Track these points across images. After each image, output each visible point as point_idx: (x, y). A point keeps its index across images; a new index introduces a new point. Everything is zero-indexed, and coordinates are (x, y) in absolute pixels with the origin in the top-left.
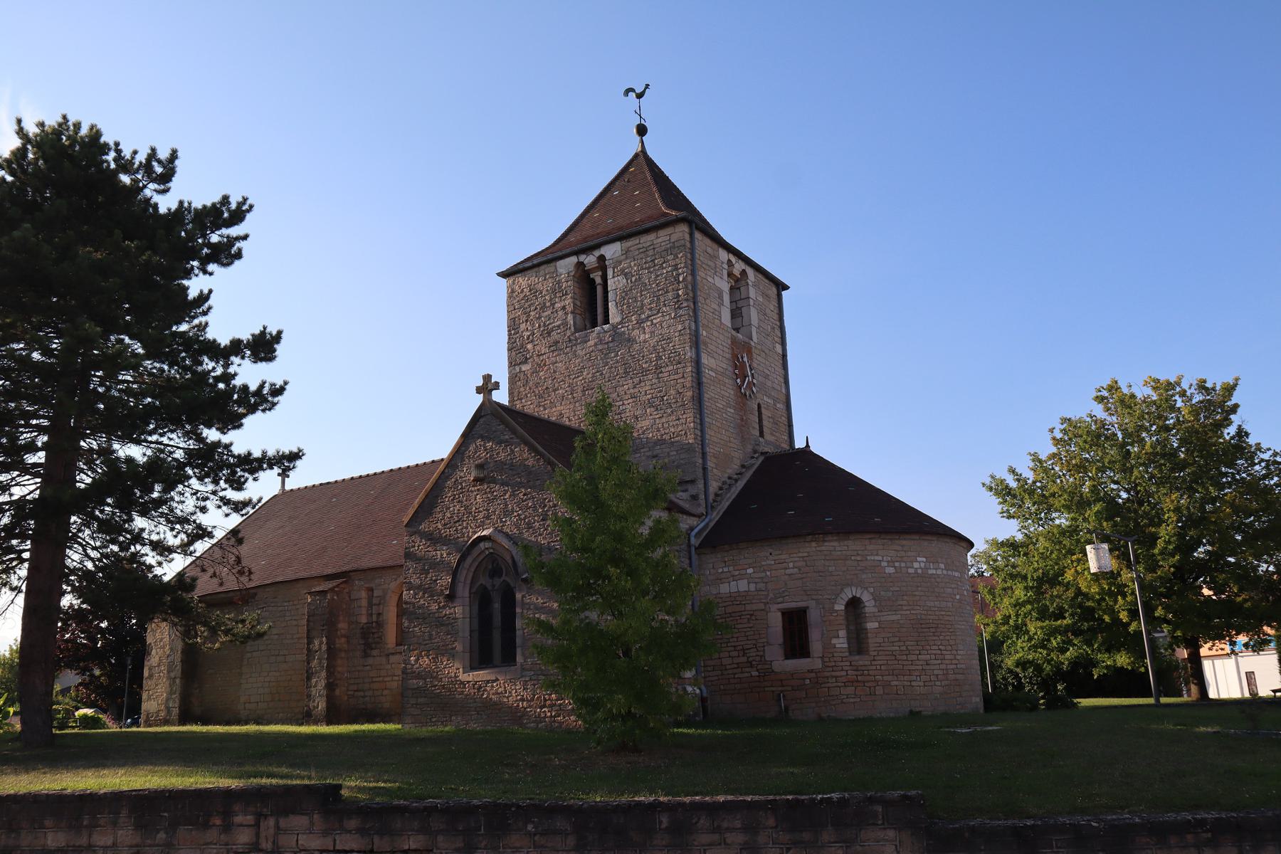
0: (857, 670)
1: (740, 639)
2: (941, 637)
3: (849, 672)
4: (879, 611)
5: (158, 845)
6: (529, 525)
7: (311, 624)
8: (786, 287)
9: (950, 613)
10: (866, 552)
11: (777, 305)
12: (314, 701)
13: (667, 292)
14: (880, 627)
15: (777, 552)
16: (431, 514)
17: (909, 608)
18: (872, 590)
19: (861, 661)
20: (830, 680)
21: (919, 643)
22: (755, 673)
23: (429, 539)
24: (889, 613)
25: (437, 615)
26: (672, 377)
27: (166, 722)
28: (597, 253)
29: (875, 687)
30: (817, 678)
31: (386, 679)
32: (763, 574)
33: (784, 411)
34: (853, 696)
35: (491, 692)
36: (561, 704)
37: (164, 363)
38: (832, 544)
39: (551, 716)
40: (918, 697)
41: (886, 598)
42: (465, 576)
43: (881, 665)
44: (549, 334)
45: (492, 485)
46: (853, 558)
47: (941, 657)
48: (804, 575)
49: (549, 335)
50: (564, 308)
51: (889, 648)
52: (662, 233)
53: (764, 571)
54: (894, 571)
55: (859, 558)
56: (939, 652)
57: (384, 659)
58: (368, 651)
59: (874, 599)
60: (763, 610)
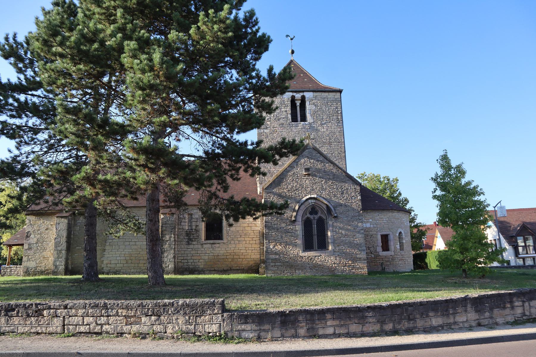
5: (486, 318)
6: (335, 196)
12: (166, 264)
13: (333, 116)
16: (280, 185)
22: (373, 256)
23: (279, 196)
25: (285, 228)
26: (336, 147)
27: (54, 273)
28: (302, 94)
31: (201, 255)
35: (318, 261)
36: (353, 265)
39: (349, 270)
42: (301, 213)
44: (279, 120)
45: (314, 177)
49: (279, 120)
50: (286, 111)
52: (330, 94)
53: (376, 221)
57: (200, 246)
58: (190, 242)
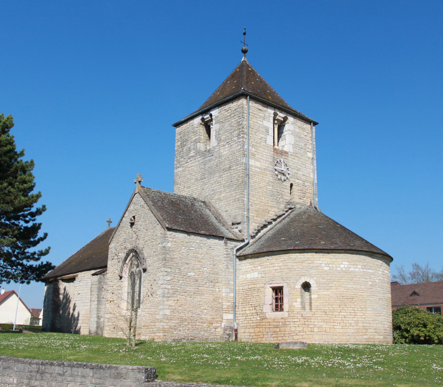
1: (254, 301)
2: (355, 304)
3: (301, 320)
7: (92, 289)
9: (363, 291)
10: (313, 259)
14: (318, 298)
17: (336, 288)
21: (340, 306)
24: (324, 290)
29: (314, 328)
30: (285, 322)
32: (264, 270)
33: (221, 212)
37: (25, 227)
40: (338, 334)
43: (317, 317)
46: (306, 262)
47: (354, 314)
48: (282, 270)
51: (323, 308)
55: (309, 262)
56: (353, 311)
59: (316, 283)
60: (263, 287)
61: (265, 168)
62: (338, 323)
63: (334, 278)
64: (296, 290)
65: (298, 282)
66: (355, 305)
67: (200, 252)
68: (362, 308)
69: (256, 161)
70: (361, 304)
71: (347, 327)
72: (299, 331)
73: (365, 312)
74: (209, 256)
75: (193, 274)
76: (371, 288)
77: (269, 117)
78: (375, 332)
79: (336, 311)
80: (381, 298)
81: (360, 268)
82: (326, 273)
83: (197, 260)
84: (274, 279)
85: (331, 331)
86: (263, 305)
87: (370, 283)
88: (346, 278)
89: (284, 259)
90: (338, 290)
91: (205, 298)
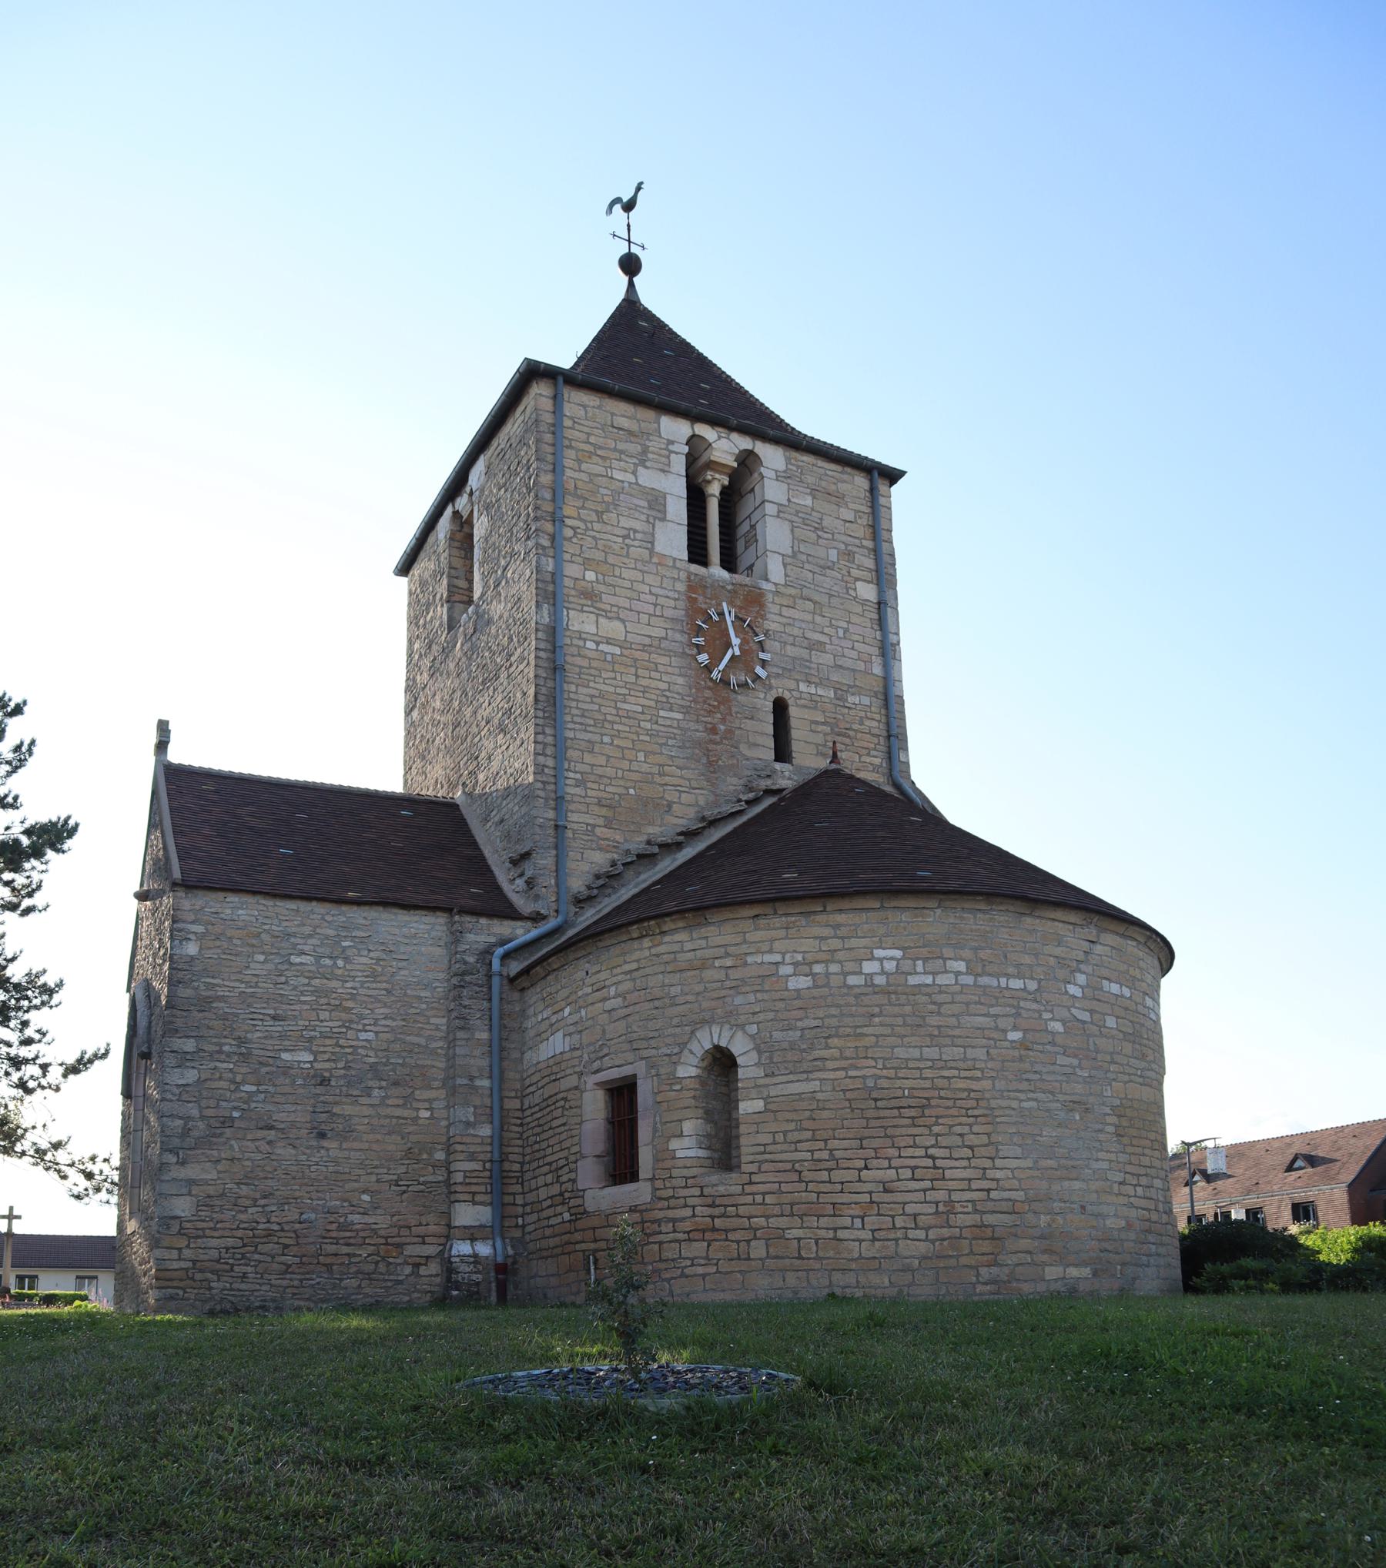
0: (712, 1205)
2: (936, 1129)
3: (698, 1210)
4: (766, 1076)
8: (893, 476)
10: (744, 948)
11: (869, 510)
14: (766, 1110)
15: (596, 968)
18: (753, 1029)
19: (726, 1184)
20: (664, 1229)
24: (791, 1077)
29: (748, 1241)
34: (703, 1262)
38: (678, 937)
40: (854, 1266)
41: (785, 1045)
43: (764, 1194)
46: (717, 963)
51: (784, 1157)
54: (810, 984)
55: (729, 963)
59: (758, 1049)
60: (576, 1088)
61: (647, 641)
62: (853, 1217)
63: (834, 1022)
64: (678, 1087)
65: (686, 1052)
66: (938, 1135)
67: (340, 972)
68: (971, 1147)
69: (601, 620)
70: (966, 1129)
71: (900, 1234)
72: (692, 1259)
73: (988, 1163)
74: (384, 985)
75: (307, 1057)
76: (1021, 1059)
77: (668, 457)
78: (1045, 1252)
79: (843, 1164)
80: (1076, 1098)
81: (958, 974)
82: (798, 1003)
83: (323, 1001)
84: (606, 1051)
85: (821, 1254)
86: (575, 1162)
87: (1015, 1036)
88: (888, 1020)
89: (638, 961)
90: (851, 1073)
91: (366, 1146)
